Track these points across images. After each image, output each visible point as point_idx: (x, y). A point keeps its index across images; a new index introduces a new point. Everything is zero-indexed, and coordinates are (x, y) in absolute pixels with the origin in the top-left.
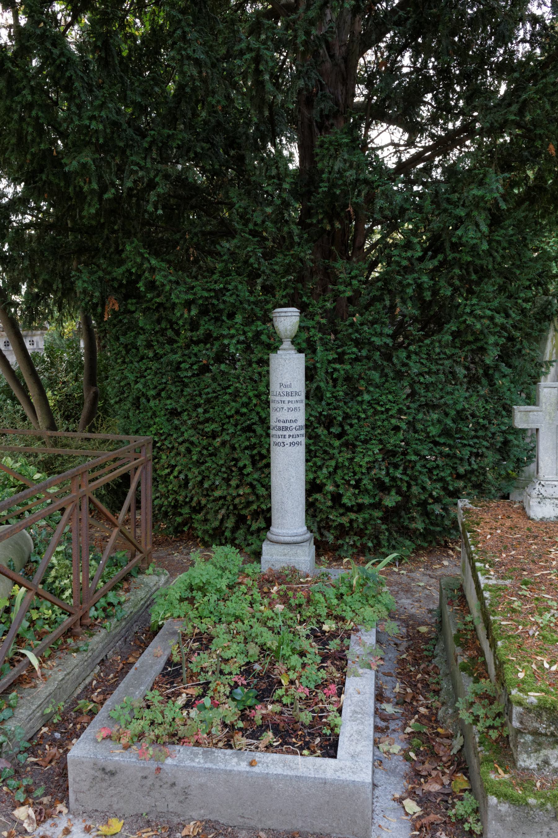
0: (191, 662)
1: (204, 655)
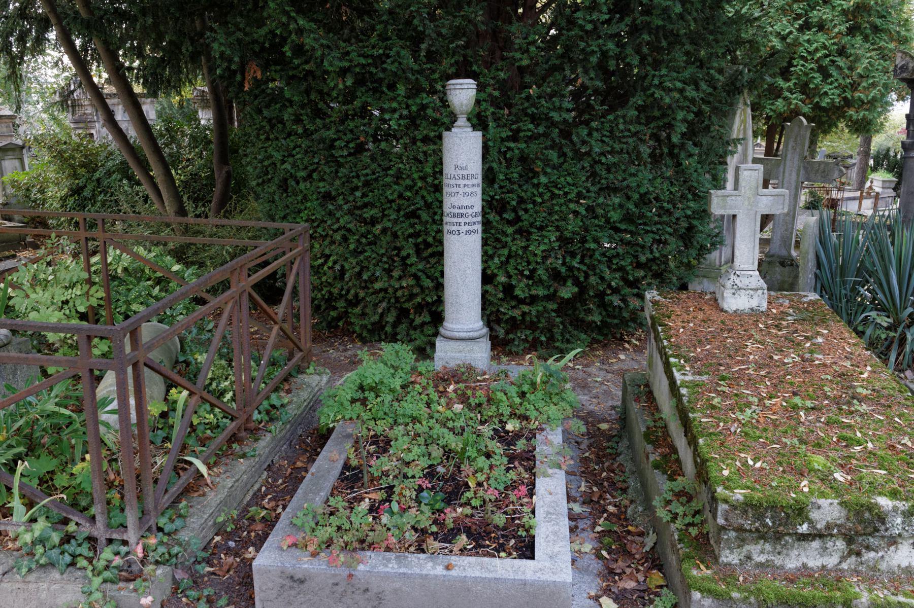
0: (370, 466)
1: (384, 459)
